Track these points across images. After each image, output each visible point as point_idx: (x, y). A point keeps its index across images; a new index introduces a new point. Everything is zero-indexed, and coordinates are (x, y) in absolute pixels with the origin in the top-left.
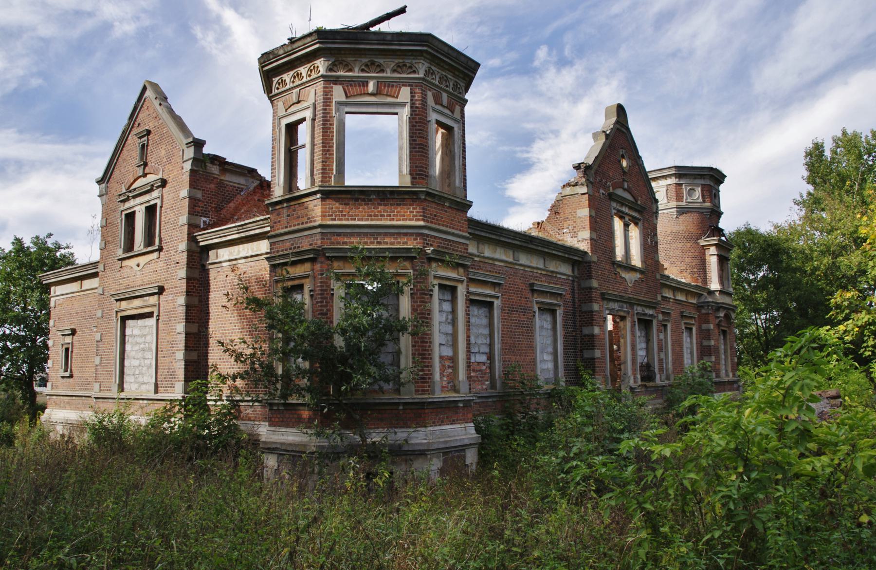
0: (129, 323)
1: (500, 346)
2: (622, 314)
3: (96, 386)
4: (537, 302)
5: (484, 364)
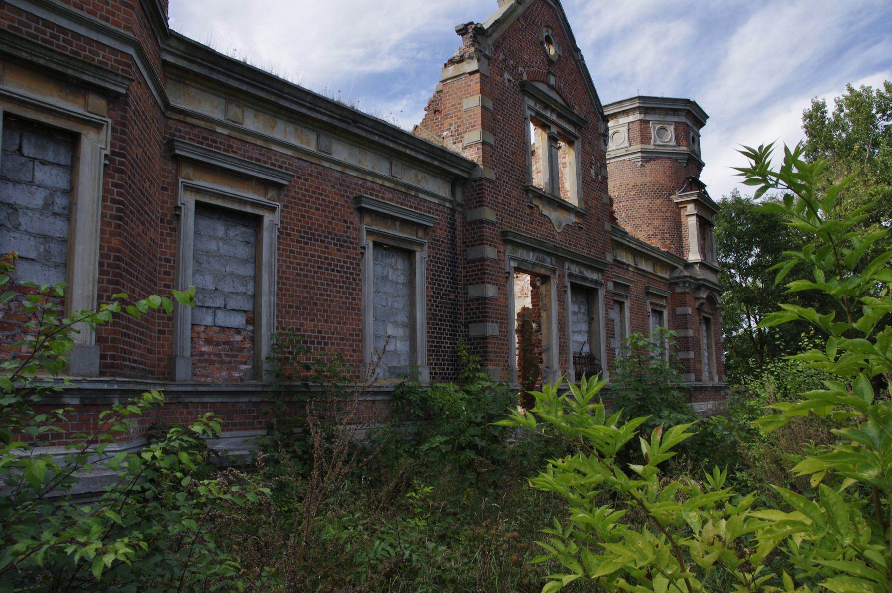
1: (274, 299)
2: (543, 271)
4: (369, 232)
5: (238, 331)
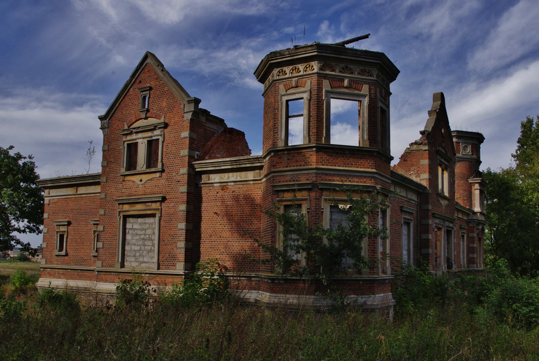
0: (131, 220)
3: (99, 263)
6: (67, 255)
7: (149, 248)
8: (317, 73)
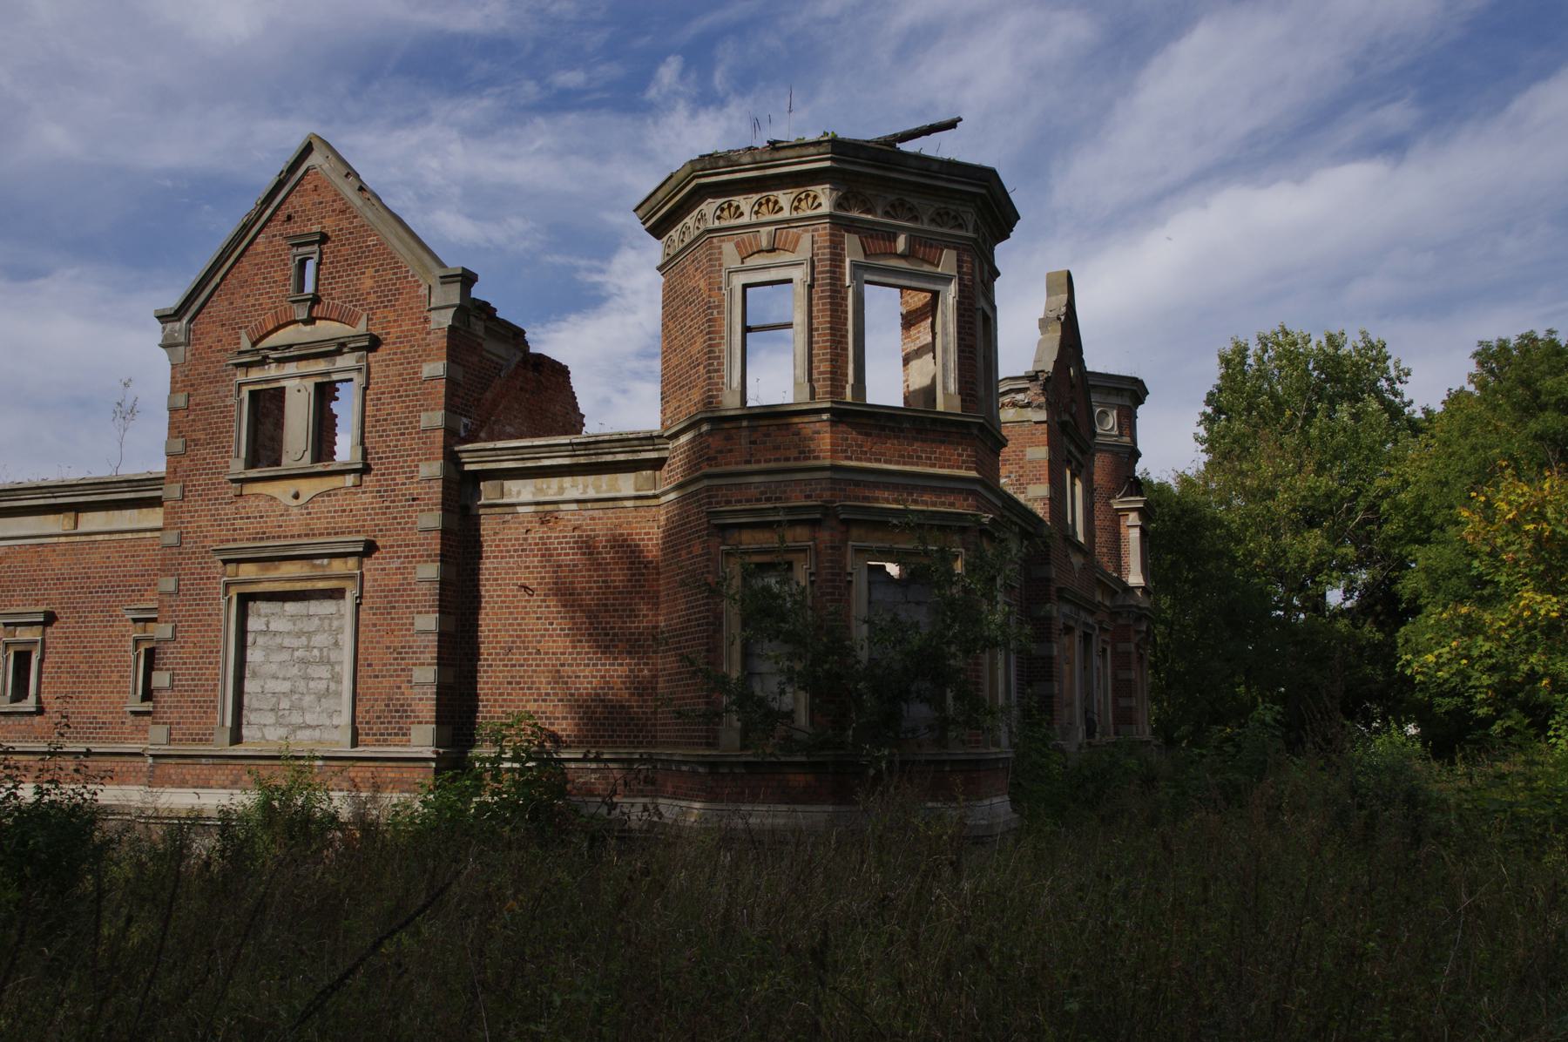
0: (263, 607)
6: (40, 711)
7: (322, 685)
8: (830, 216)
